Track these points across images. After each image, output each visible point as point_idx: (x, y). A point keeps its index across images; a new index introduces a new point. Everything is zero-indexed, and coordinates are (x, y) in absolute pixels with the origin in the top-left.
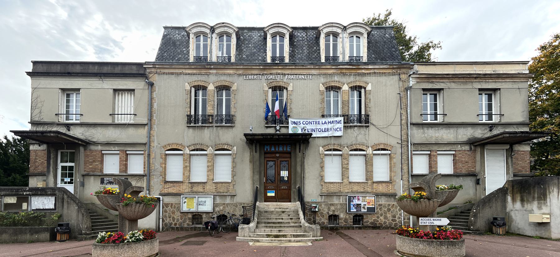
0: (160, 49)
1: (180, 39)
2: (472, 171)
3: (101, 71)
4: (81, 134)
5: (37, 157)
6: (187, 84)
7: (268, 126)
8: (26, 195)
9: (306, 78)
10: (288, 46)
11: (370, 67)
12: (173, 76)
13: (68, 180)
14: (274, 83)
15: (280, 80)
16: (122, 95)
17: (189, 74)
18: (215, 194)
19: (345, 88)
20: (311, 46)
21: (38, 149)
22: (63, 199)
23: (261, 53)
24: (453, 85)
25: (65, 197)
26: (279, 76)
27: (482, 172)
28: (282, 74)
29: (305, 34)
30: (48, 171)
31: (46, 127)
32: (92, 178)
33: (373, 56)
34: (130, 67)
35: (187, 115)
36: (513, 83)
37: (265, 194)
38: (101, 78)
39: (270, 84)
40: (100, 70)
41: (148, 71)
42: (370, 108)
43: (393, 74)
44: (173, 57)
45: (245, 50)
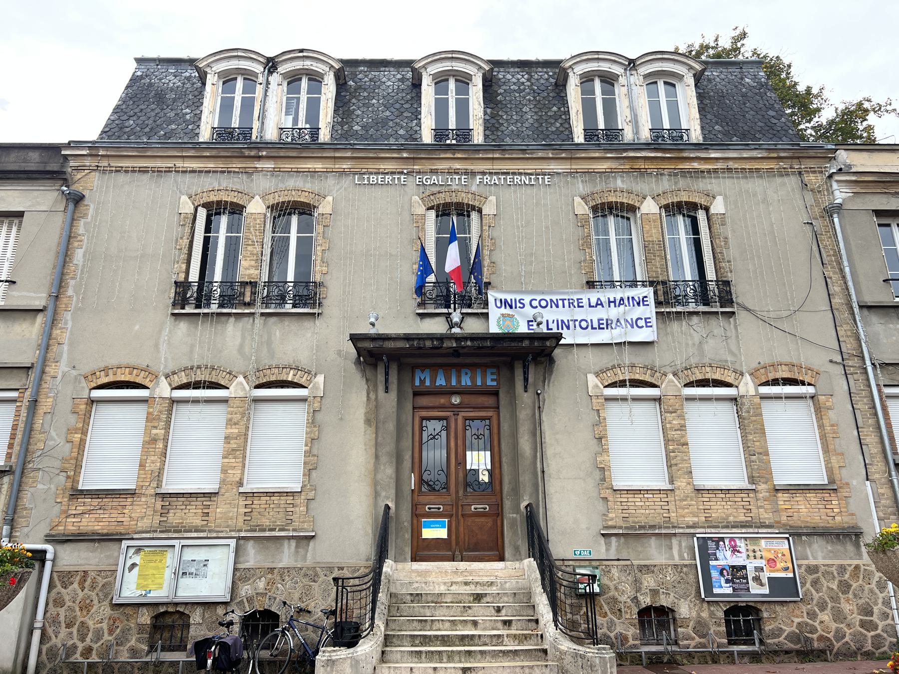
1: (178, 87)
6: (184, 198)
7: (426, 311)
9: (533, 183)
10: (480, 104)
11: (713, 155)
12: (146, 177)
14: (442, 195)
17: (191, 172)
18: (243, 534)
19: (649, 207)
26: (457, 177)
28: (466, 173)
29: (526, 76)
32: (653, 541)
34: (22, 154)
35: (176, 282)
39: (432, 197)
43: (783, 173)
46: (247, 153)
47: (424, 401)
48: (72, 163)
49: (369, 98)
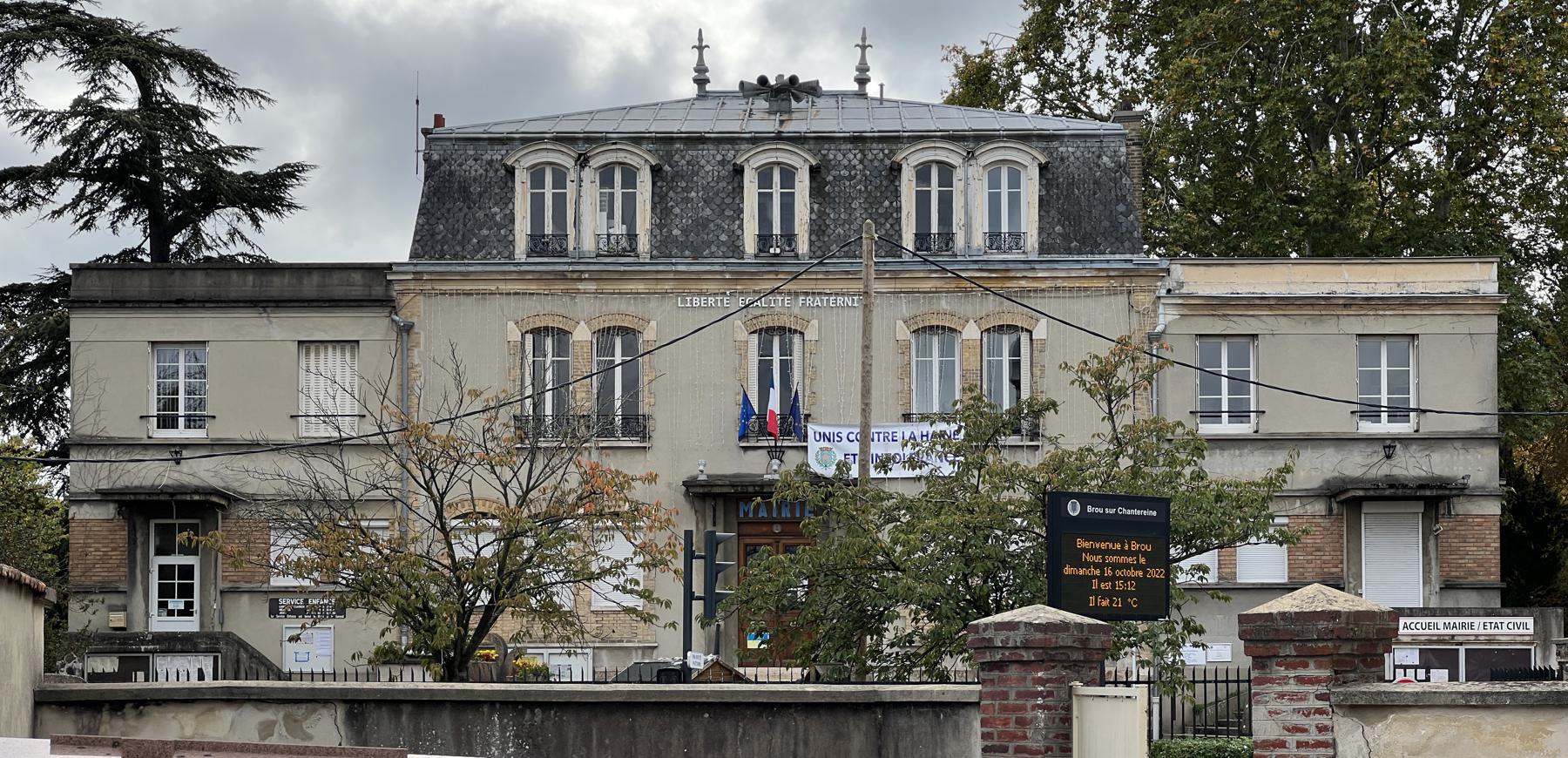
0: (423, 211)
1: (481, 175)
2: (1332, 574)
3: (263, 289)
4: (212, 474)
5: (89, 541)
6: (511, 324)
7: (748, 445)
8: (147, 651)
9: (856, 305)
10: (805, 205)
11: (1039, 275)
12: (470, 299)
13: (177, 604)
14: (764, 319)
15: (782, 309)
16: (317, 354)
17: (515, 294)
18: (597, 645)
19: (971, 332)
20: (876, 197)
21: (92, 517)
22: (238, 661)
23: (727, 222)
24: (1282, 325)
25: (244, 655)
26: (780, 299)
27: (1351, 580)
28: (789, 294)
29: (859, 156)
30: (132, 583)
31: (113, 453)
32: (245, 599)
33: (1058, 229)
34: (344, 274)
35: (514, 416)
36: (1455, 319)
37: (742, 643)
38: (265, 312)
39: (754, 321)
40: (261, 286)
41: (396, 288)
42: (1042, 392)
43: (1113, 292)
44: (463, 235)
45: (677, 210)
46: (569, 276)
47: (748, 529)
48: (397, 287)
49: (687, 190)
